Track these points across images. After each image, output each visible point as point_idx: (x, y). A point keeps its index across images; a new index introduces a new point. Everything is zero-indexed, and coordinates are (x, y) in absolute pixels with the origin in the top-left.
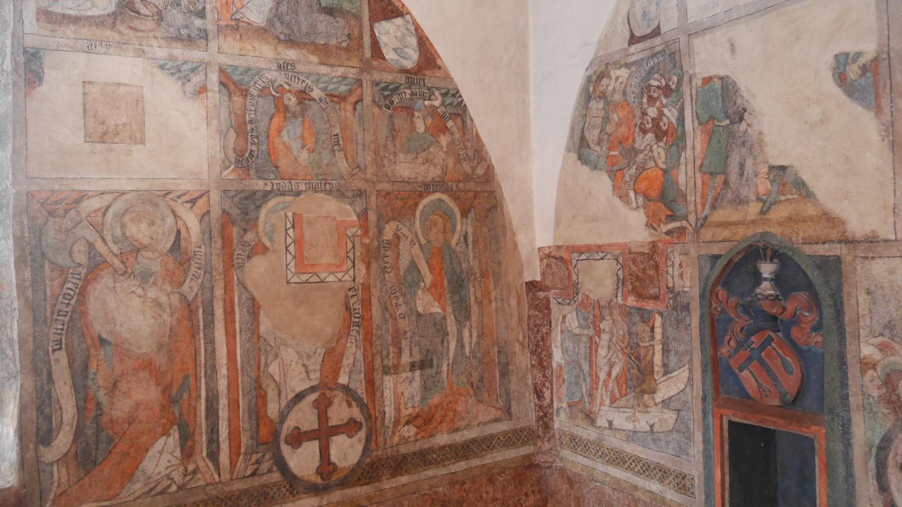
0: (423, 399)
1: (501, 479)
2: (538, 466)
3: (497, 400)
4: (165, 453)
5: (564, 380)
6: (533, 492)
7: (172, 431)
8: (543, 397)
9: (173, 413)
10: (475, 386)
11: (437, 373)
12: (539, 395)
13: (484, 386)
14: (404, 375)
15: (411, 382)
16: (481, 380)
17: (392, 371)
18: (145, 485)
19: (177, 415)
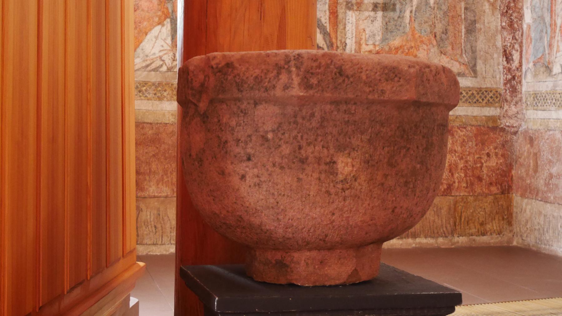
0: (384, 40)
1: (462, 134)
2: (503, 130)
3: (461, 55)
4: (160, 39)
5: (531, 39)
6: (496, 154)
7: (165, 22)
8: (513, 60)
9: (167, 8)
10: (438, 37)
11: (399, 17)
12: (508, 57)
13: (448, 38)
14: (367, 14)
15: (372, 21)
16: (445, 32)
17: (355, 8)
18: (144, 61)
19: (170, 11)
